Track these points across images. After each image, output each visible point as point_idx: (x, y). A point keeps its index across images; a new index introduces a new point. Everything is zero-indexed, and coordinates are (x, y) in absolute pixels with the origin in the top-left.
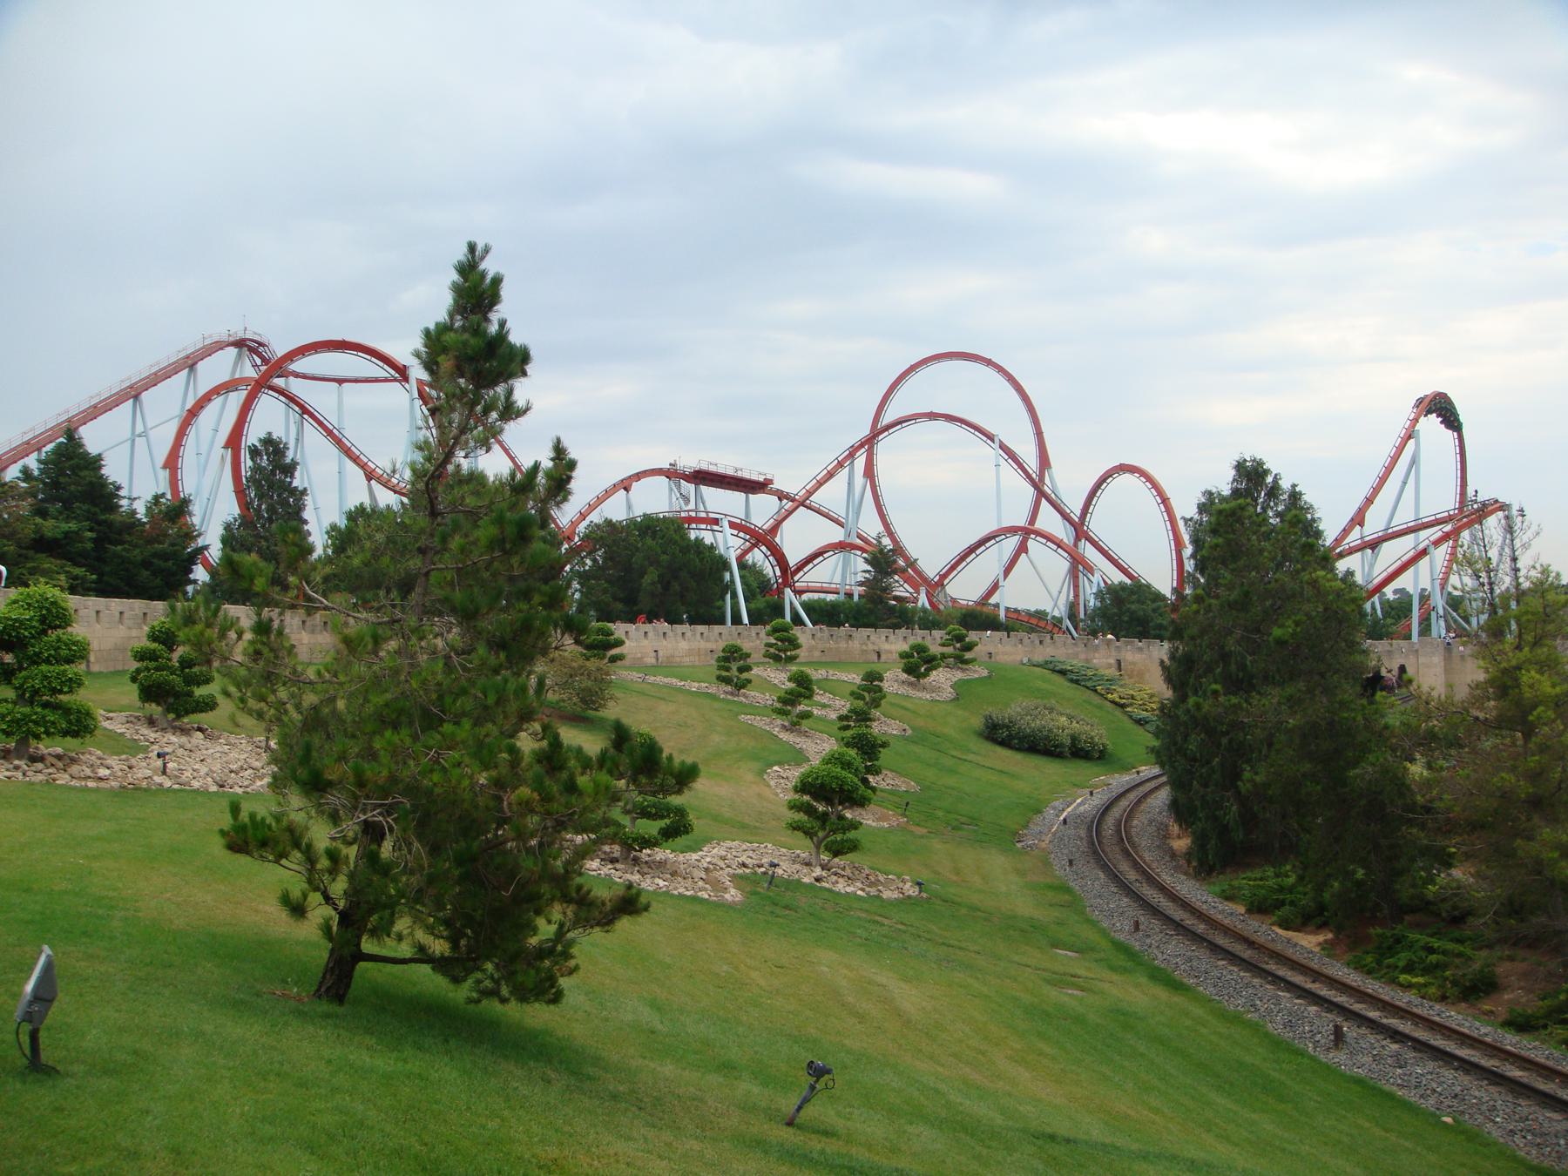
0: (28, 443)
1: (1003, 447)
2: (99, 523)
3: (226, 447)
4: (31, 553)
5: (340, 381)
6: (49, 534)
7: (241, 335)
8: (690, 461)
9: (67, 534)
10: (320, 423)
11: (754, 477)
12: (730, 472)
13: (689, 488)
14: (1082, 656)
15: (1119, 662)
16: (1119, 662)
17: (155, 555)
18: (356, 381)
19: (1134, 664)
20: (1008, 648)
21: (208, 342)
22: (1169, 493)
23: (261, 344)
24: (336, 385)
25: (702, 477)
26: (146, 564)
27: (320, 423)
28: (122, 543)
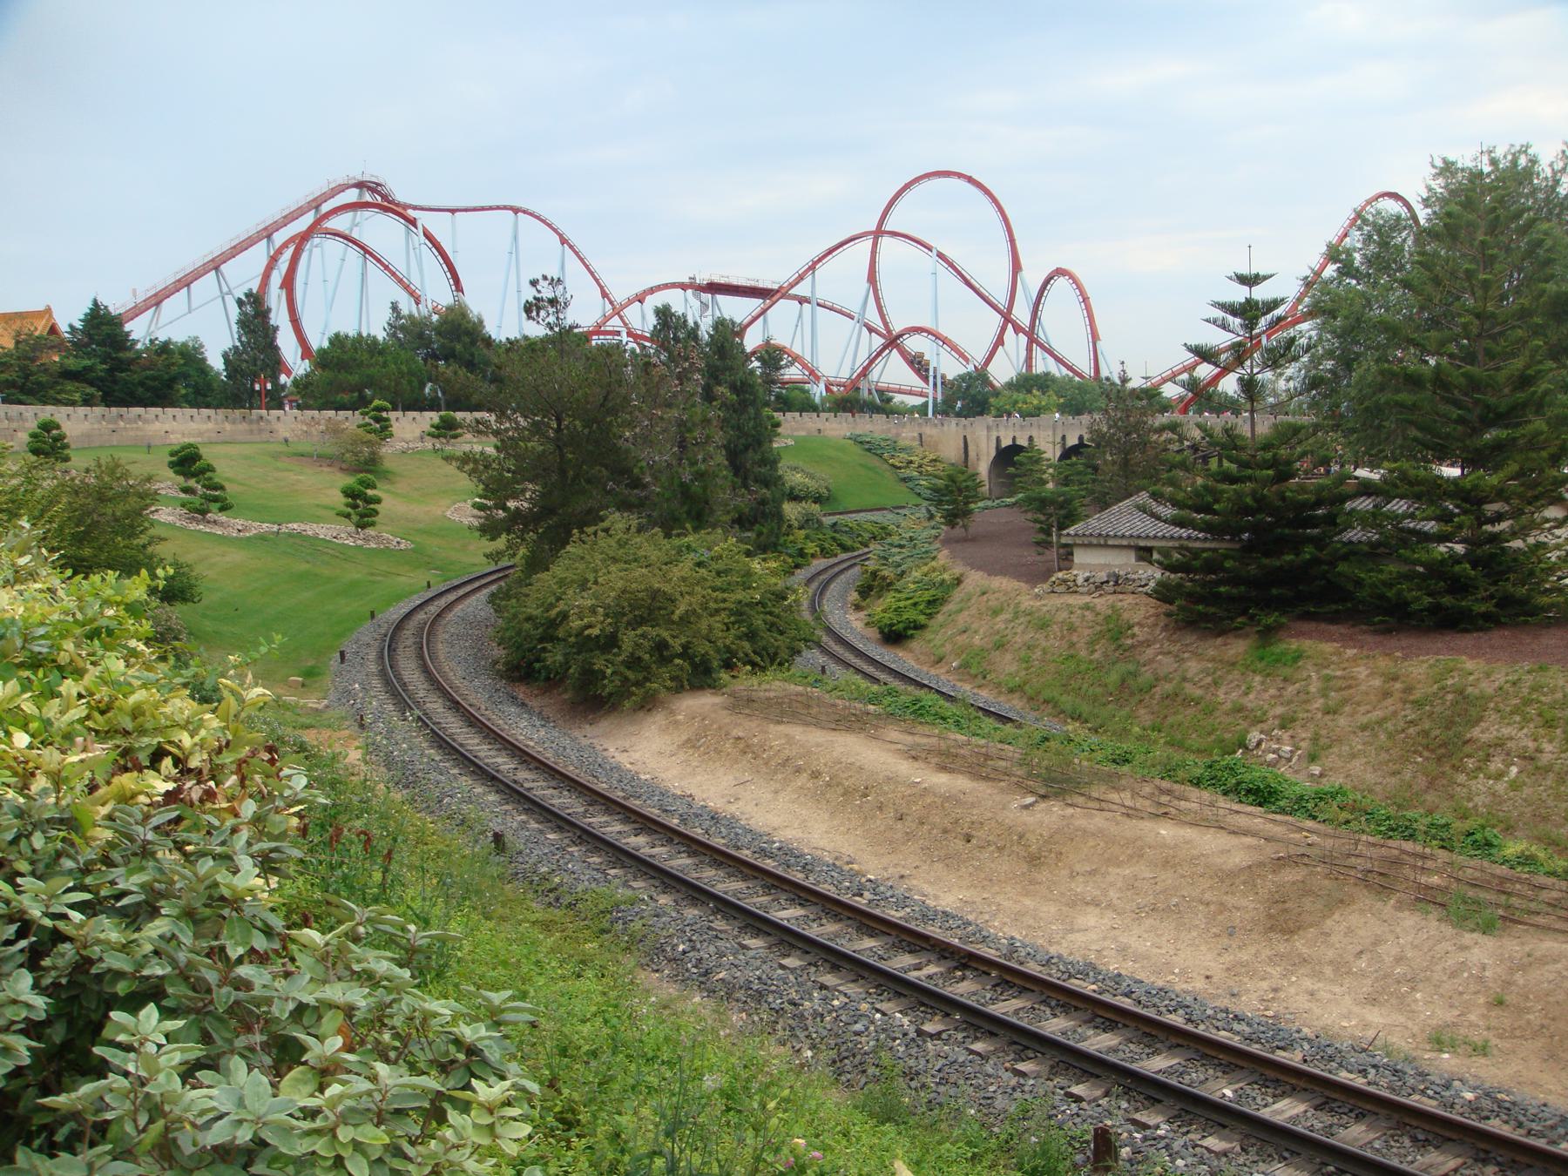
0: (179, 281)
1: (940, 255)
2: (113, 359)
3: (281, 288)
4: (61, 380)
5: (453, 211)
6: (73, 368)
7: (360, 178)
8: (703, 278)
9: (85, 368)
10: (378, 260)
11: (769, 286)
12: (722, 281)
13: (707, 297)
14: (894, 431)
15: (921, 435)
16: (921, 435)
17: (147, 378)
18: (466, 210)
19: (931, 436)
20: (835, 425)
21: (333, 185)
22: (1090, 293)
23: (378, 184)
24: (449, 214)
25: (715, 288)
26: (142, 384)
27: (378, 260)
28: (127, 370)
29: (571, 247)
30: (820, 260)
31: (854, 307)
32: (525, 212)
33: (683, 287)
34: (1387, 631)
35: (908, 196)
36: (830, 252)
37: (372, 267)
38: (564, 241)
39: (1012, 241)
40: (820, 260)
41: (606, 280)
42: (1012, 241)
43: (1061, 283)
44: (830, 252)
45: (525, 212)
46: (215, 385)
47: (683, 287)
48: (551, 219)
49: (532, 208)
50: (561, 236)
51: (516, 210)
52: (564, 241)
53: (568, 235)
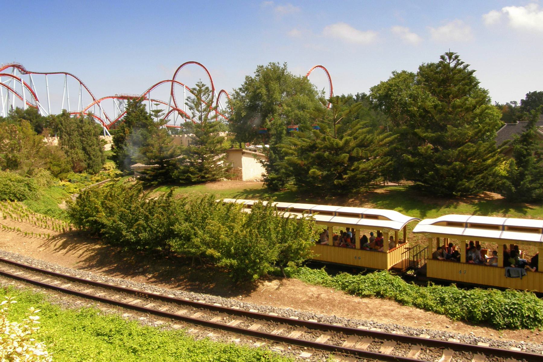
5: (46, 74)
8: (119, 95)
13: (121, 100)
23: (20, 66)
29: (83, 85)
30: (151, 89)
31: (167, 101)
32: (69, 74)
33: (113, 97)
34: (191, 186)
35: (182, 69)
36: (154, 86)
37: (10, 91)
38: (81, 83)
39: (212, 82)
40: (151, 89)
41: (94, 95)
42: (212, 82)
43: (223, 94)
44: (154, 86)
45: (69, 74)
46: (523, 106)
47: (113, 97)
48: (75, 75)
49: (73, 74)
50: (80, 82)
51: (66, 74)
52: (81, 83)
53: (82, 81)
